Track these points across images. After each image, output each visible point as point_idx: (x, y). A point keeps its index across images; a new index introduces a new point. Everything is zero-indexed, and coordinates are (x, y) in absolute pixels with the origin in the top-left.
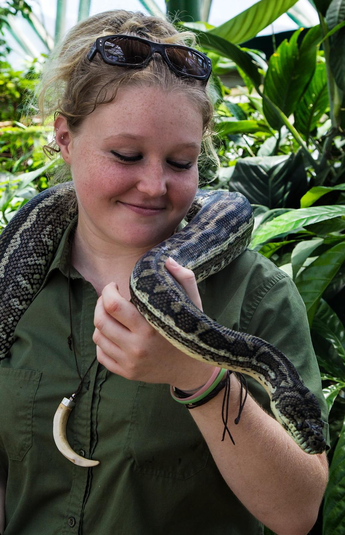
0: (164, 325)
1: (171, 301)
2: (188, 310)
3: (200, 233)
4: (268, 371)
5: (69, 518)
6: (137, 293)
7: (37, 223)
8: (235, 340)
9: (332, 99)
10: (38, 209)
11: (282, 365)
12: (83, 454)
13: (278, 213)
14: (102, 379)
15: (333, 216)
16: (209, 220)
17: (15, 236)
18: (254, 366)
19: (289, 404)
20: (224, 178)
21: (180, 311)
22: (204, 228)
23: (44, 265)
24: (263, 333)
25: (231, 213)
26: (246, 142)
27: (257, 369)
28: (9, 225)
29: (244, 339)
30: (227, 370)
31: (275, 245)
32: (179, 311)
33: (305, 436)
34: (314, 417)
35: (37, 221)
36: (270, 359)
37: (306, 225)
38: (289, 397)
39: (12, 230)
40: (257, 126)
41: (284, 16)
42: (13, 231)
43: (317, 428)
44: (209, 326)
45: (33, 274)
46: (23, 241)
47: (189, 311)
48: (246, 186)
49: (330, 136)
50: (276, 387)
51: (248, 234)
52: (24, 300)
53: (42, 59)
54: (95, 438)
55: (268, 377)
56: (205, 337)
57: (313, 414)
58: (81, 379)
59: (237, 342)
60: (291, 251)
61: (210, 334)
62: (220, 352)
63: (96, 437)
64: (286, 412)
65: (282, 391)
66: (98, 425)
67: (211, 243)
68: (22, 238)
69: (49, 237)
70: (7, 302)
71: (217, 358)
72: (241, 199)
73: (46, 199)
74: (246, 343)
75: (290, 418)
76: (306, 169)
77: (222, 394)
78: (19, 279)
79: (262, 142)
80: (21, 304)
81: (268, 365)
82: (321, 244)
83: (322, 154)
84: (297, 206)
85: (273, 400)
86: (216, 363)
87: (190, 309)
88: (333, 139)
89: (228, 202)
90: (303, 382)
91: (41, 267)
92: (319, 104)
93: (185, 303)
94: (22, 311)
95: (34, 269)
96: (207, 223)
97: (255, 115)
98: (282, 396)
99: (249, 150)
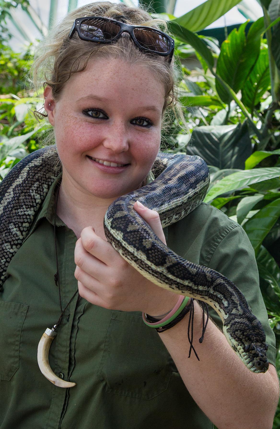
2: (157, 246)
3: (164, 186)
4: (222, 300)
8: (197, 272)
9: (273, 79)
11: (234, 295)
12: (62, 377)
14: (80, 312)
16: (172, 177)
17: (9, 191)
18: (211, 295)
19: (239, 329)
20: (183, 143)
22: (167, 183)
23: (33, 216)
25: (191, 172)
26: (202, 113)
27: (213, 298)
29: (203, 271)
31: (223, 200)
32: (150, 247)
33: (251, 357)
34: (259, 341)
35: (28, 177)
37: (249, 184)
38: (238, 323)
39: (7, 185)
40: (211, 101)
41: (234, 10)
42: (7, 185)
43: (261, 351)
44: (175, 260)
45: (22, 223)
46: (15, 195)
47: (158, 247)
48: (201, 150)
49: (271, 109)
50: (228, 314)
52: (15, 244)
55: (222, 305)
56: (172, 270)
59: (198, 274)
60: (236, 205)
61: (177, 267)
62: (185, 282)
64: (235, 335)
65: (233, 318)
67: (173, 195)
68: (15, 192)
69: (37, 191)
72: (200, 161)
73: (35, 159)
75: (239, 341)
76: (251, 136)
78: (10, 227)
79: (215, 113)
80: (12, 248)
81: (222, 295)
82: (261, 199)
84: (243, 167)
85: (225, 325)
86: (180, 291)
87: (159, 245)
88: (274, 112)
89: (189, 163)
90: (251, 311)
91: (30, 217)
93: (154, 240)
94: (13, 254)
95: (24, 219)
96: (170, 179)
97: (210, 91)
98: (233, 322)
99: (204, 120)
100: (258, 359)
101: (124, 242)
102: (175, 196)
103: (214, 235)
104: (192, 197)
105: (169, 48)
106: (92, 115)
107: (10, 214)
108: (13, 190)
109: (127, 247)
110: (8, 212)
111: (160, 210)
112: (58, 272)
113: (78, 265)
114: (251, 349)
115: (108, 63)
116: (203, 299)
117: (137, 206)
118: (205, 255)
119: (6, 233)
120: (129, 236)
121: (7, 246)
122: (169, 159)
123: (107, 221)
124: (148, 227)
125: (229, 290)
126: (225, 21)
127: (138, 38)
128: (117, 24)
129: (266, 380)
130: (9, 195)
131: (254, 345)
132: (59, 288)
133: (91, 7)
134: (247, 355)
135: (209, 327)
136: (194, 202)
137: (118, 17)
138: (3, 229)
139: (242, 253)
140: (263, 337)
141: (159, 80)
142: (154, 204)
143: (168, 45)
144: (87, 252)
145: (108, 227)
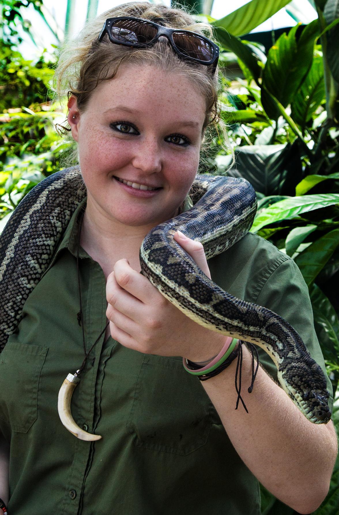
0: (178, 296)
1: (186, 273)
3: (206, 213)
4: (276, 342)
5: (70, 491)
6: (150, 265)
7: (46, 205)
8: (247, 310)
9: (328, 91)
10: (48, 191)
11: (290, 337)
13: (274, 200)
14: (106, 356)
15: (327, 204)
16: (214, 202)
17: (25, 217)
18: (263, 336)
19: (296, 375)
20: (223, 165)
21: (195, 283)
23: (53, 246)
24: (274, 305)
25: (235, 197)
26: (244, 131)
28: (19, 206)
30: (238, 340)
31: (270, 231)
32: (194, 282)
33: (311, 406)
36: (279, 330)
38: (296, 367)
39: (23, 211)
40: (255, 116)
41: (283, 10)
42: (23, 212)
43: (323, 398)
44: (223, 296)
45: (41, 254)
46: (33, 222)
47: (203, 282)
48: (244, 173)
49: (325, 126)
50: (283, 357)
51: (252, 217)
52: (32, 279)
53: (52, 50)
54: (99, 413)
55: (276, 347)
56: (219, 308)
57: (319, 385)
58: (86, 355)
60: (285, 237)
61: (224, 304)
62: (233, 322)
63: (99, 412)
64: (293, 381)
65: (289, 362)
66: (102, 401)
67: (216, 222)
68: (32, 219)
69: (58, 218)
70: (16, 280)
71: (230, 328)
72: (245, 184)
73: (56, 182)
74: (257, 313)
76: (302, 158)
77: (235, 362)
78: (27, 259)
79: (259, 131)
80: (29, 283)
81: (276, 336)
83: (317, 145)
84: (293, 194)
85: (280, 370)
86: (228, 333)
87: (204, 280)
89: (233, 186)
92: (316, 96)
94: (30, 290)
95: (43, 250)
96: (212, 205)
97: (253, 106)
98: (289, 366)
99: (247, 139)
100: (319, 408)
101: (163, 276)
102: (218, 224)
103: (261, 269)
104: (237, 225)
105: (212, 56)
106: (121, 130)
107: (27, 244)
108: (30, 217)
109: (167, 282)
110: (25, 242)
111: (203, 240)
112: (81, 310)
113: (111, 304)
114: (311, 397)
115: (142, 70)
116: (254, 341)
117: (178, 235)
118: (251, 291)
119: (22, 266)
120: (169, 270)
121: (23, 281)
122: (209, 181)
123: (144, 253)
124: (190, 259)
125: (284, 331)
126: (272, 25)
127: (178, 43)
128: (154, 26)
129: (323, 436)
130: (25, 222)
131: (314, 392)
132: (83, 329)
133: (126, 7)
134: (306, 403)
135: (259, 375)
136: (240, 231)
137: (156, 19)
138: (19, 261)
139: (293, 289)
140: (324, 383)
141: (199, 92)
142: (195, 234)
143: (211, 53)
144: (122, 289)
145: (145, 259)
